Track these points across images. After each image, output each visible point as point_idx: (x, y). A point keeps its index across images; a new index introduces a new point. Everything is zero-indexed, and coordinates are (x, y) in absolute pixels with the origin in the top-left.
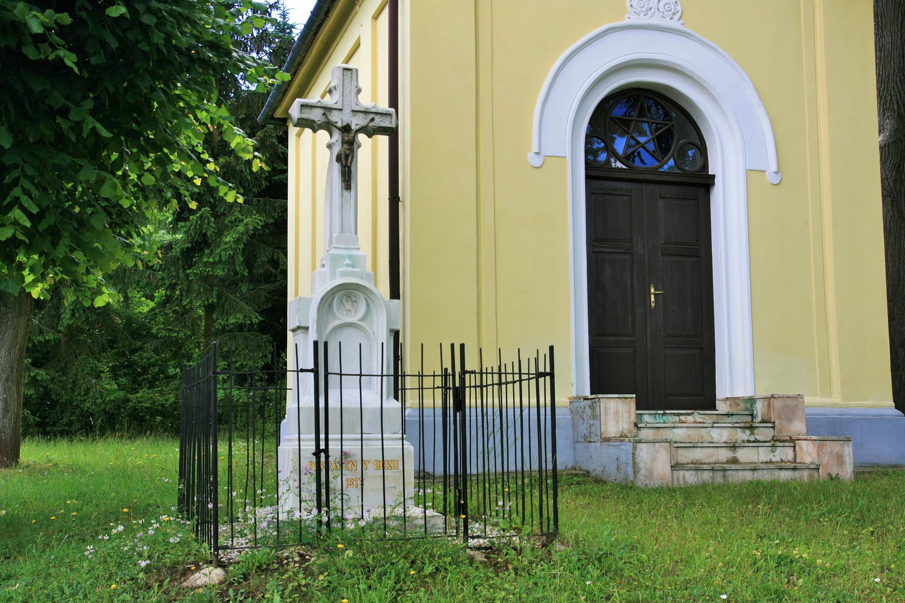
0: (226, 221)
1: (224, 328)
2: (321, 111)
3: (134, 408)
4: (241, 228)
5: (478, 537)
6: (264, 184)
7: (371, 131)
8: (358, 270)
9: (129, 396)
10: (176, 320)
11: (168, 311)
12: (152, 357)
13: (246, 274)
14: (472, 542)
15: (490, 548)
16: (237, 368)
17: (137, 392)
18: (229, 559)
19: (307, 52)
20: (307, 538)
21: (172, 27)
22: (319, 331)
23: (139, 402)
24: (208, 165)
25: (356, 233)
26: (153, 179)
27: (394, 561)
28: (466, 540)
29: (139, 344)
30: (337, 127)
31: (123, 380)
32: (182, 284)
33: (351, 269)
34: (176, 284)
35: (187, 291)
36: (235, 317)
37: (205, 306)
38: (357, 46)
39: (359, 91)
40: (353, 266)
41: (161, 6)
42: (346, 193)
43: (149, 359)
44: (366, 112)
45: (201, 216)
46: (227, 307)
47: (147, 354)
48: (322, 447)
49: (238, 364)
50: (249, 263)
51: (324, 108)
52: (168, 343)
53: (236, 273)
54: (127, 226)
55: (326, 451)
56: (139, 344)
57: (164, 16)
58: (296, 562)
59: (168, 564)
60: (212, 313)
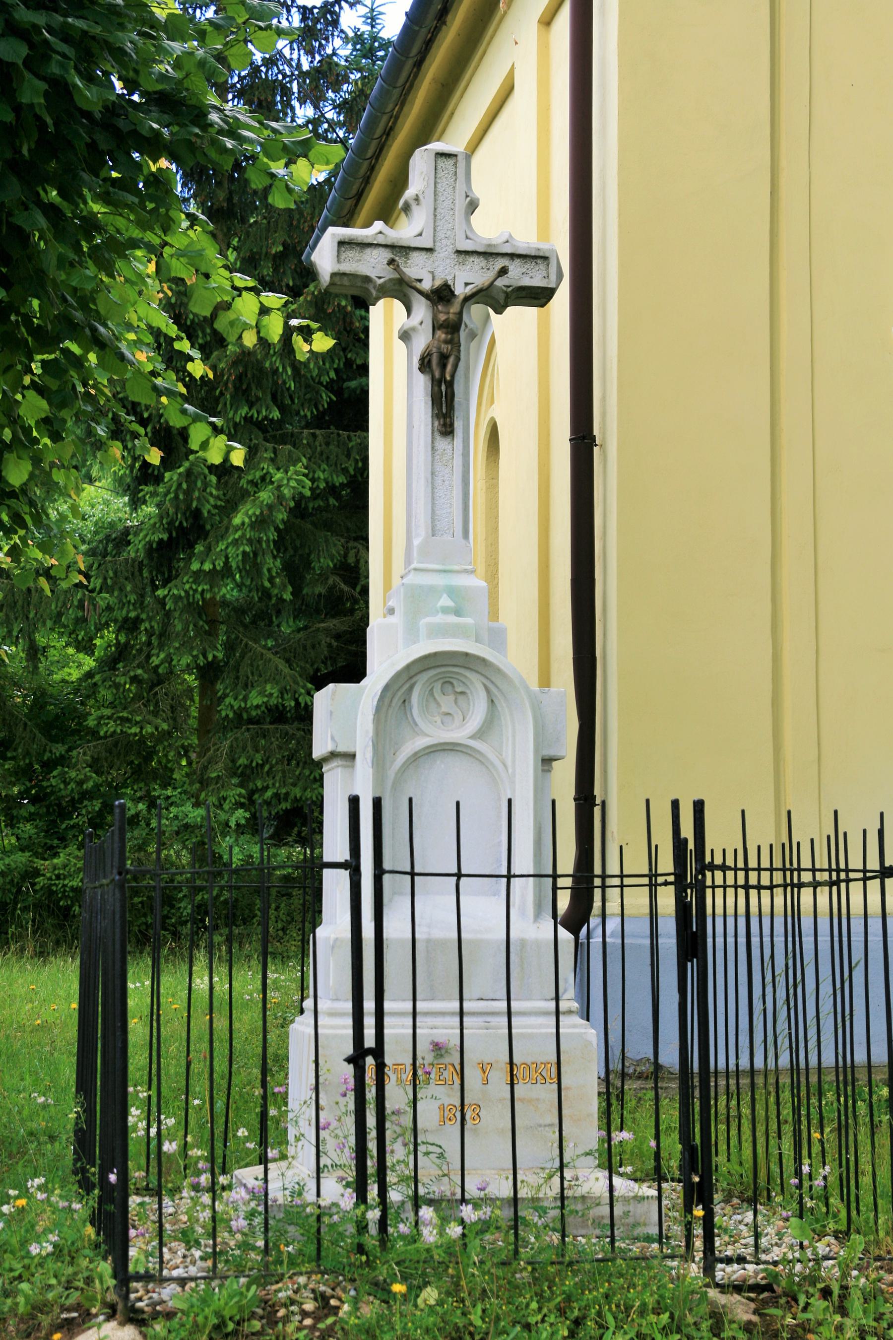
0: (243, 482)
1: (238, 715)
2: (387, 255)
3: (49, 892)
4: (265, 496)
5: (741, 1260)
6: (326, 397)
7: (501, 298)
8: (468, 620)
9: (39, 863)
10: (138, 697)
11: (122, 680)
12: (87, 779)
13: (287, 596)
14: (722, 1272)
15: (769, 1288)
16: (268, 803)
17: (56, 855)
18: (154, 1305)
19: (403, 104)
20: (339, 1251)
21: (62, 66)
22: (380, 762)
23: (58, 877)
24: (190, 366)
25: (466, 534)
26: (44, 404)
27: (532, 1320)
28: (708, 1269)
29: (59, 749)
30: (420, 292)
31: (28, 829)
32: (150, 619)
33: (452, 619)
34: (137, 621)
35: (160, 636)
36: (262, 693)
37: (198, 667)
38: (507, 91)
39: (473, 206)
40: (458, 612)
41: (39, 18)
42: (442, 443)
43: (80, 783)
44: (488, 255)
45: (189, 473)
46: (245, 669)
47: (79, 773)
48: (370, 1042)
49: (269, 794)
50: (295, 572)
51: (392, 247)
52: (120, 747)
53: (266, 594)
54: (12, 502)
55: (378, 1052)
56: (59, 749)
57: (46, 41)
58: (305, 1314)
59: (21, 1309)
60: (213, 683)
